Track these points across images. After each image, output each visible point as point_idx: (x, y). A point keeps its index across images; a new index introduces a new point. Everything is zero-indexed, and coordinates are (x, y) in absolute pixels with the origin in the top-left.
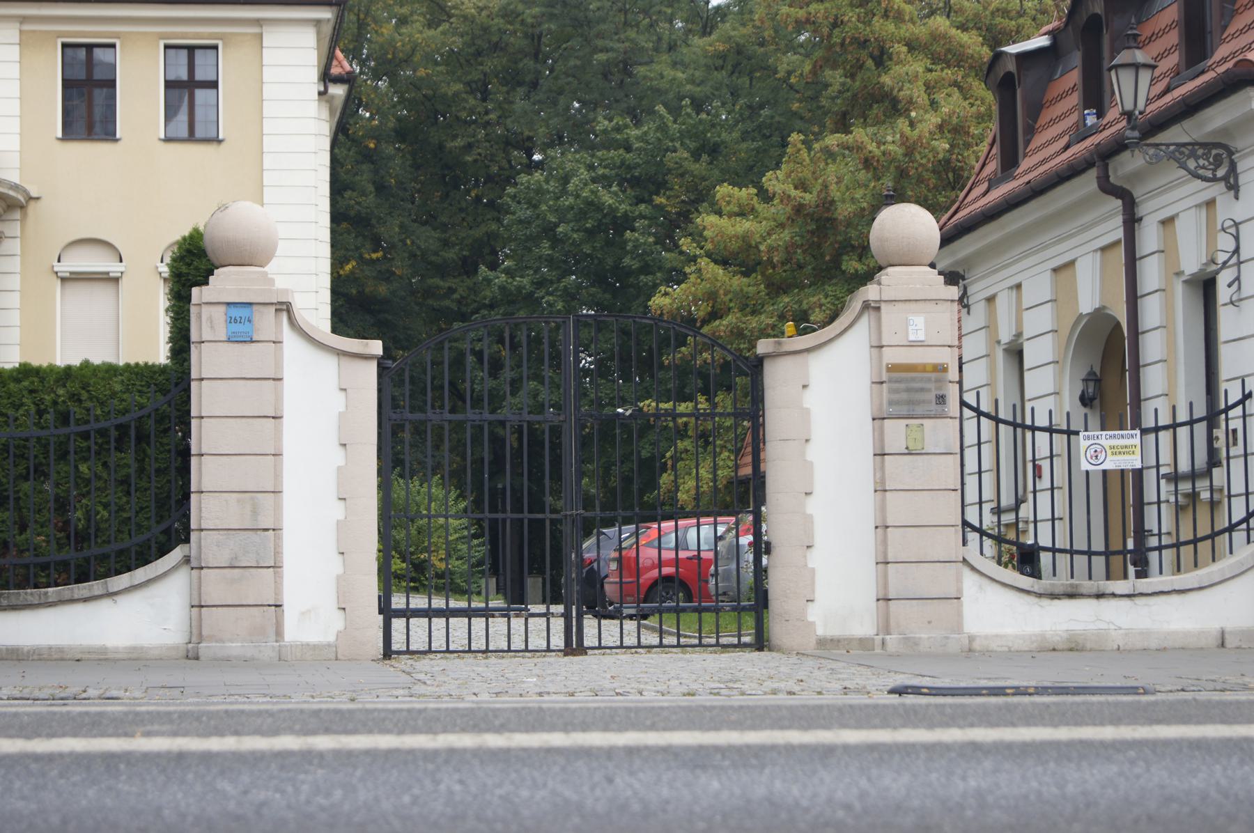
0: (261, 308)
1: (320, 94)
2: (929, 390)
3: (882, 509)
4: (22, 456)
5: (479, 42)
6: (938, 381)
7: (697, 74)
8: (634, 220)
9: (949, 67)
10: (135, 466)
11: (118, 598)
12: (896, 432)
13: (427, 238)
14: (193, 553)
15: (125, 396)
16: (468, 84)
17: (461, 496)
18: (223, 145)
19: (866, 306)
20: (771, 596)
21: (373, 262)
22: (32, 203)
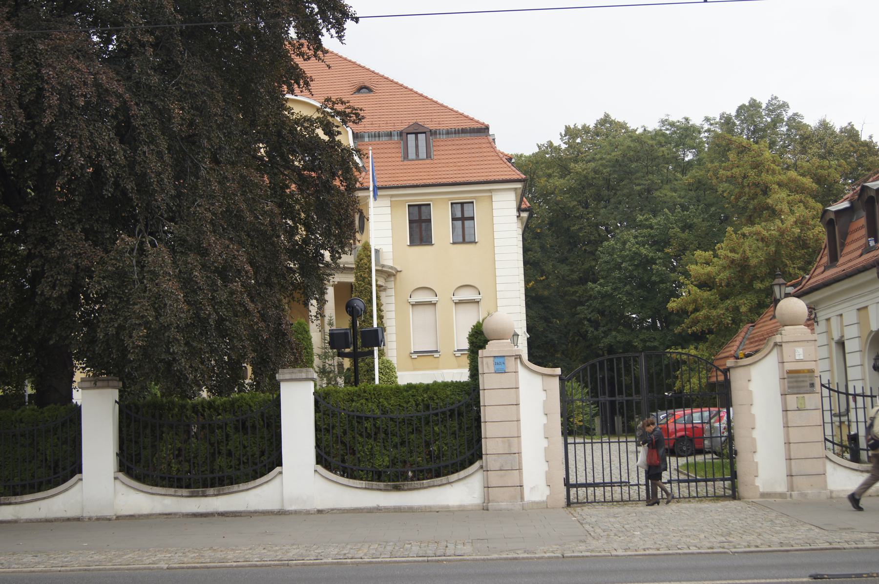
0: (509, 358)
1: (518, 217)
2: (806, 381)
3: (787, 435)
4: (410, 424)
5: (583, 183)
6: (810, 377)
7: (682, 193)
8: (656, 259)
9: (798, 194)
10: (457, 426)
11: (453, 484)
12: (792, 400)
13: (564, 269)
14: (484, 465)
15: (452, 396)
16: (579, 201)
17: (586, 386)
18: (478, 244)
19: (776, 344)
20: (738, 474)
21: (541, 281)
22: (398, 273)
